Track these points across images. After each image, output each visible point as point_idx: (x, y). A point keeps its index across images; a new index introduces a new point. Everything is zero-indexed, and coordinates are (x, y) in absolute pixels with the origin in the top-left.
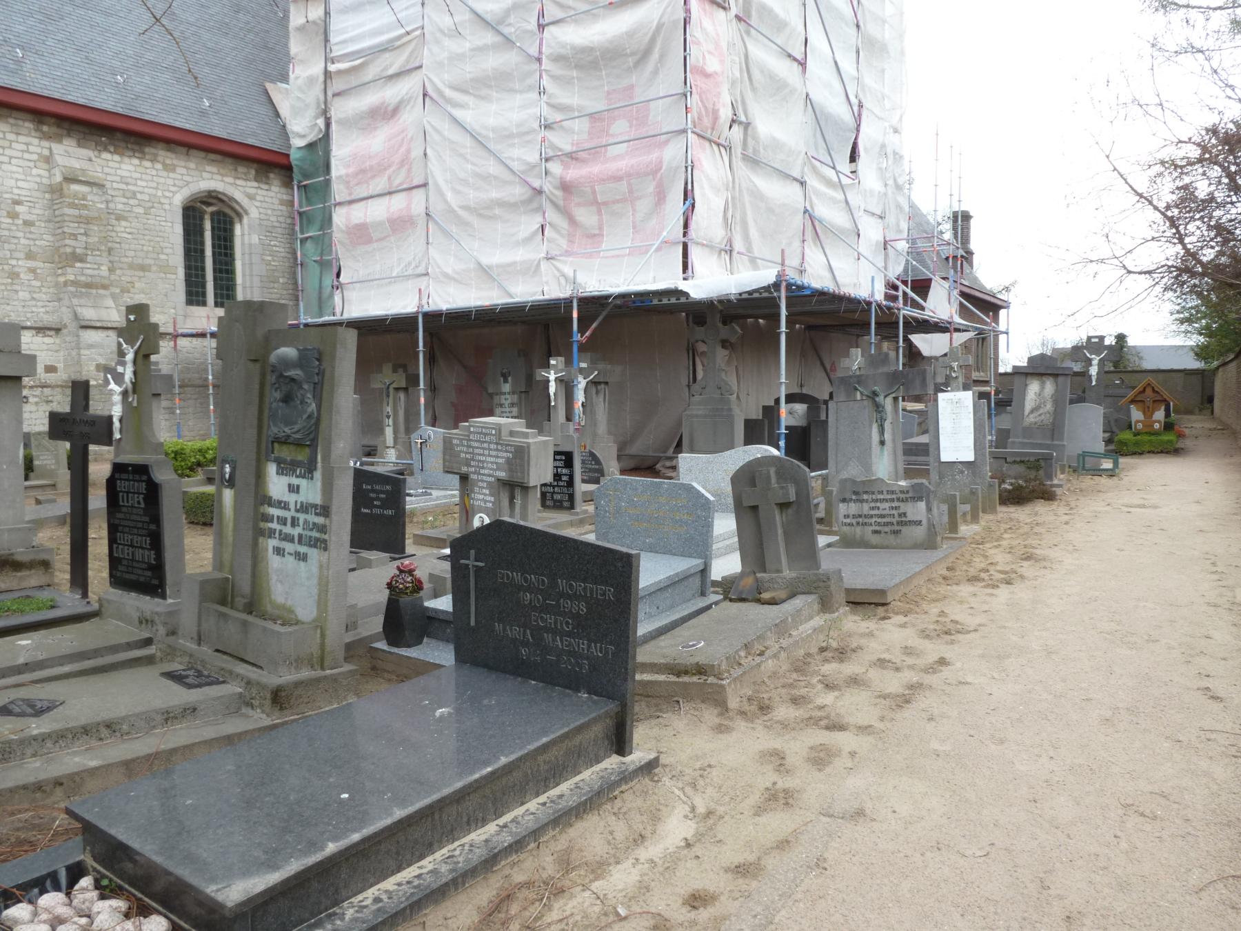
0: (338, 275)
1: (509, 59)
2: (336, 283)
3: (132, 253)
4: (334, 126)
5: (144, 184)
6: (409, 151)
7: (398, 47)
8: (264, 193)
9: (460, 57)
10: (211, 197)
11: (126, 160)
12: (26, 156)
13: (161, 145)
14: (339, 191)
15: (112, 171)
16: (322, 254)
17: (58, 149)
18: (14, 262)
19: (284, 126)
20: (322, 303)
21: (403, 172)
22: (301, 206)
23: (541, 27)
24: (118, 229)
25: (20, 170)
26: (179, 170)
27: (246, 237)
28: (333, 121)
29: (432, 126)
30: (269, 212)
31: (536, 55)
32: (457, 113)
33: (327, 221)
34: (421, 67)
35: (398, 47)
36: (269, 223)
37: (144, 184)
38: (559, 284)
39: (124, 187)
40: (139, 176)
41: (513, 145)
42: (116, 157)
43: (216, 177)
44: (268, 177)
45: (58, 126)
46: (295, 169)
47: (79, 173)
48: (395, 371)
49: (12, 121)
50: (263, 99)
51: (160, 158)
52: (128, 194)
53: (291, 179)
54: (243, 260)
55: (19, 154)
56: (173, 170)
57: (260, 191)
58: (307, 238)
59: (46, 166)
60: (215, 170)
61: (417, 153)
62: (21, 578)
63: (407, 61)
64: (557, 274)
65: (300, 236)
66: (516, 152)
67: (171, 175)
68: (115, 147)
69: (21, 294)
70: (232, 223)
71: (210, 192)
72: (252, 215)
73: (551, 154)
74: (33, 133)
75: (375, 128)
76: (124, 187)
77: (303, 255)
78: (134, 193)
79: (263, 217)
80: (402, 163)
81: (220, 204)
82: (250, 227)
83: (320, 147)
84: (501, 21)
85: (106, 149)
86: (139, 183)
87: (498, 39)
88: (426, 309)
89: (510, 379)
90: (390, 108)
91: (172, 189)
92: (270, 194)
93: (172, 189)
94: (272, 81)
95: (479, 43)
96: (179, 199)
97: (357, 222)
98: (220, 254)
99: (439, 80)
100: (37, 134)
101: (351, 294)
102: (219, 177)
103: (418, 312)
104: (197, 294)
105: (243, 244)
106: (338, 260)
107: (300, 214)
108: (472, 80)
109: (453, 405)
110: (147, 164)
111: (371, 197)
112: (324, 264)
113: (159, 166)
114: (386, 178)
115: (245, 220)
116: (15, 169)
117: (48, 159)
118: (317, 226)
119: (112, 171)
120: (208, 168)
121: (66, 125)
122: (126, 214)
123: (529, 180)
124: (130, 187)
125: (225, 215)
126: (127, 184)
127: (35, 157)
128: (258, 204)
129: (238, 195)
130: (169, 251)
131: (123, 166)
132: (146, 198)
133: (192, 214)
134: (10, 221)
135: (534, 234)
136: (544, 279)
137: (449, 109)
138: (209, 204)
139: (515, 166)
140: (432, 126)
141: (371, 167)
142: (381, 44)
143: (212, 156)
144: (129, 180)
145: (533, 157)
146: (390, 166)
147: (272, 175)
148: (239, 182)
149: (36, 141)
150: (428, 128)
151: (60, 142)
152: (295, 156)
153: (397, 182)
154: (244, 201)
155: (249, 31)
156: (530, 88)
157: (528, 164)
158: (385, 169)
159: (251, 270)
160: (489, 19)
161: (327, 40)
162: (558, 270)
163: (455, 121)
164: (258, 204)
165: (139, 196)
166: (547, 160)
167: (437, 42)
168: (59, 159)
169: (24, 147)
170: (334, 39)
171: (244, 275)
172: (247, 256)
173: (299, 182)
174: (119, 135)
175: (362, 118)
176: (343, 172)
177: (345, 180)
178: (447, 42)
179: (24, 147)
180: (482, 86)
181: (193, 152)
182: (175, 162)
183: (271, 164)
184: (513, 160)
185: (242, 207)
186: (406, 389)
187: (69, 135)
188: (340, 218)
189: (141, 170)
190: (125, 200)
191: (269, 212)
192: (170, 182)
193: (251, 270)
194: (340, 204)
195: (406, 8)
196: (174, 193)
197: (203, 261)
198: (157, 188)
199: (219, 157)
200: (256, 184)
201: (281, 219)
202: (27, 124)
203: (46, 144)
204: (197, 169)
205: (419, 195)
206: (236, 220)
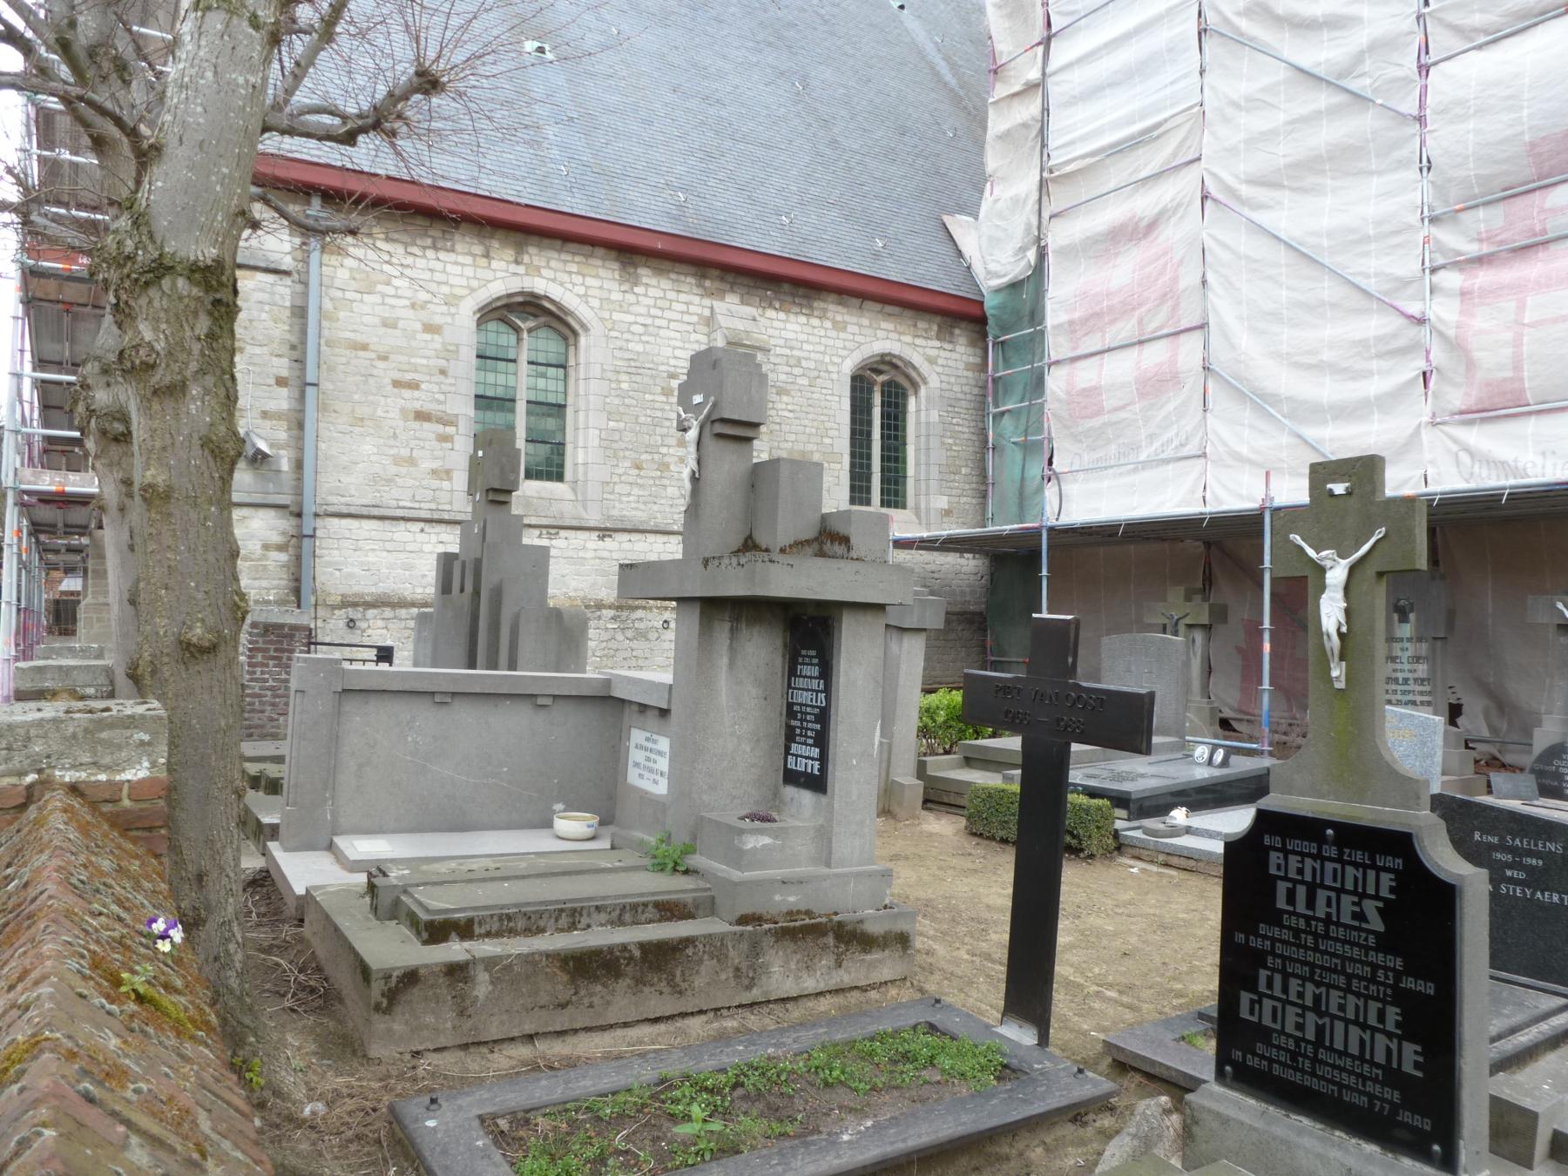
0: (1050, 463)
1: (1364, 123)
2: (1047, 472)
3: (793, 437)
4: (1051, 258)
5: (810, 347)
6: (1175, 280)
7: (1158, 137)
8: (948, 354)
9: (1270, 135)
10: (885, 363)
11: (792, 317)
12: (686, 318)
13: (833, 297)
14: (1056, 346)
15: (776, 333)
16: (1026, 433)
17: (719, 306)
18: (664, 450)
19: (969, 268)
20: (1025, 498)
21: (1164, 311)
22: (996, 370)
23: (1424, 69)
24: (779, 406)
25: (678, 335)
26: (850, 328)
27: (923, 414)
28: (1050, 250)
29: (1216, 240)
30: (953, 380)
31: (1415, 112)
32: (1260, 217)
33: (1038, 384)
34: (1199, 159)
35: (1158, 137)
36: (952, 395)
37: (810, 347)
38: (1458, 463)
39: (788, 352)
40: (804, 337)
41: (1367, 254)
42: (782, 315)
43: (892, 335)
44: (952, 334)
45: (722, 279)
46: (991, 321)
47: (743, 335)
48: (1188, 599)
49: (673, 276)
50: (942, 235)
51: (830, 315)
52: (792, 362)
53: (985, 335)
54: (917, 444)
55: (679, 317)
56: (844, 329)
57: (942, 353)
58: (1003, 413)
59: (705, 330)
60: (890, 326)
61: (1189, 279)
62: (872, 965)
63: (1175, 155)
64: (1455, 448)
65: (993, 410)
66: (1372, 264)
67: (842, 335)
68: (781, 301)
69: (669, 490)
70: (905, 396)
71: (883, 355)
72: (932, 385)
73: (1441, 261)
74: (695, 290)
75: (1117, 255)
76: (788, 352)
77: (998, 435)
78: (799, 359)
79: (945, 386)
80: (1164, 297)
81: (893, 372)
82: (928, 399)
83: (1028, 290)
84: (1346, 73)
85: (771, 306)
86: (805, 346)
87: (1341, 98)
88: (1278, 502)
89: (1412, 616)
90: (1144, 223)
91: (842, 352)
92: (954, 356)
93: (842, 352)
94: (951, 214)
95: (1305, 110)
96: (848, 367)
97: (1084, 386)
98: (889, 437)
99: (1225, 171)
100: (700, 291)
101: (1070, 488)
102: (895, 336)
103: (1262, 509)
104: (861, 489)
105: (918, 423)
106: (1050, 440)
107: (995, 381)
108: (1289, 166)
109: (1239, 650)
110: (815, 322)
111: (1109, 350)
112: (1029, 448)
113: (828, 324)
114: (1134, 321)
115: (923, 391)
116: (672, 334)
117: (710, 321)
118: (1016, 397)
119: (776, 333)
120: (884, 325)
121: (730, 278)
122: (788, 387)
123: (1399, 304)
124: (795, 353)
125: (897, 385)
126: (792, 348)
127: (695, 319)
128: (939, 369)
129: (917, 359)
130: (835, 433)
131: (789, 326)
132: (812, 365)
133: (860, 385)
134: (663, 399)
135: (1410, 383)
136: (1427, 456)
137: (1246, 212)
138: (880, 372)
139: (1371, 285)
140: (1216, 240)
141: (1111, 309)
142: (1132, 137)
143: (889, 309)
144: (794, 343)
145: (1408, 266)
146: (1140, 305)
147: (957, 331)
148: (919, 341)
149: (696, 299)
150: (1209, 243)
151: (723, 299)
152: (991, 303)
153: (1153, 326)
154: (924, 367)
155: (917, 156)
156: (1402, 164)
157: (1397, 279)
158: (1134, 309)
159: (928, 456)
160: (1322, 75)
161: (1044, 145)
162: (1455, 441)
163: (1261, 229)
164: (939, 369)
165: (804, 364)
166: (1433, 271)
167: (1226, 120)
168: (723, 321)
169: (684, 307)
170: (1053, 143)
171: (917, 464)
172: (923, 439)
173: (996, 337)
174: (786, 287)
175: (1096, 242)
176: (1063, 318)
177: (1071, 327)
178: (1243, 119)
179: (684, 307)
180: (1301, 175)
181: (868, 304)
182: (847, 318)
183: (961, 315)
184: (1368, 276)
185: (919, 374)
186: (1207, 628)
187: (732, 291)
188: (1055, 382)
189: (808, 329)
190: (788, 369)
191: (953, 380)
192: (839, 344)
193: (928, 456)
194: (1057, 362)
195: (1172, 83)
196: (844, 358)
197: (869, 447)
198: (824, 353)
199: (896, 310)
200: (937, 344)
201: (966, 389)
202: (689, 279)
203: (707, 302)
204: (870, 326)
205: (1192, 343)
206: (911, 392)
